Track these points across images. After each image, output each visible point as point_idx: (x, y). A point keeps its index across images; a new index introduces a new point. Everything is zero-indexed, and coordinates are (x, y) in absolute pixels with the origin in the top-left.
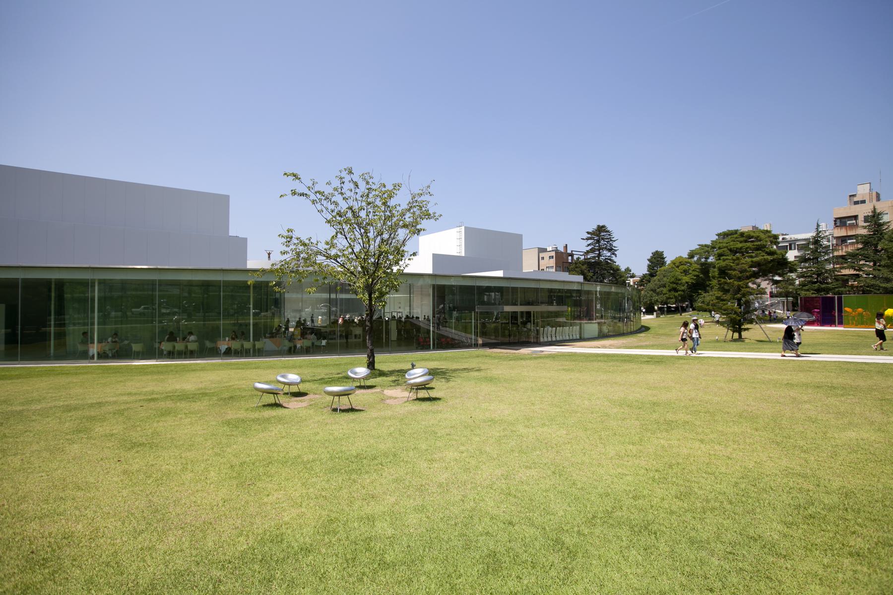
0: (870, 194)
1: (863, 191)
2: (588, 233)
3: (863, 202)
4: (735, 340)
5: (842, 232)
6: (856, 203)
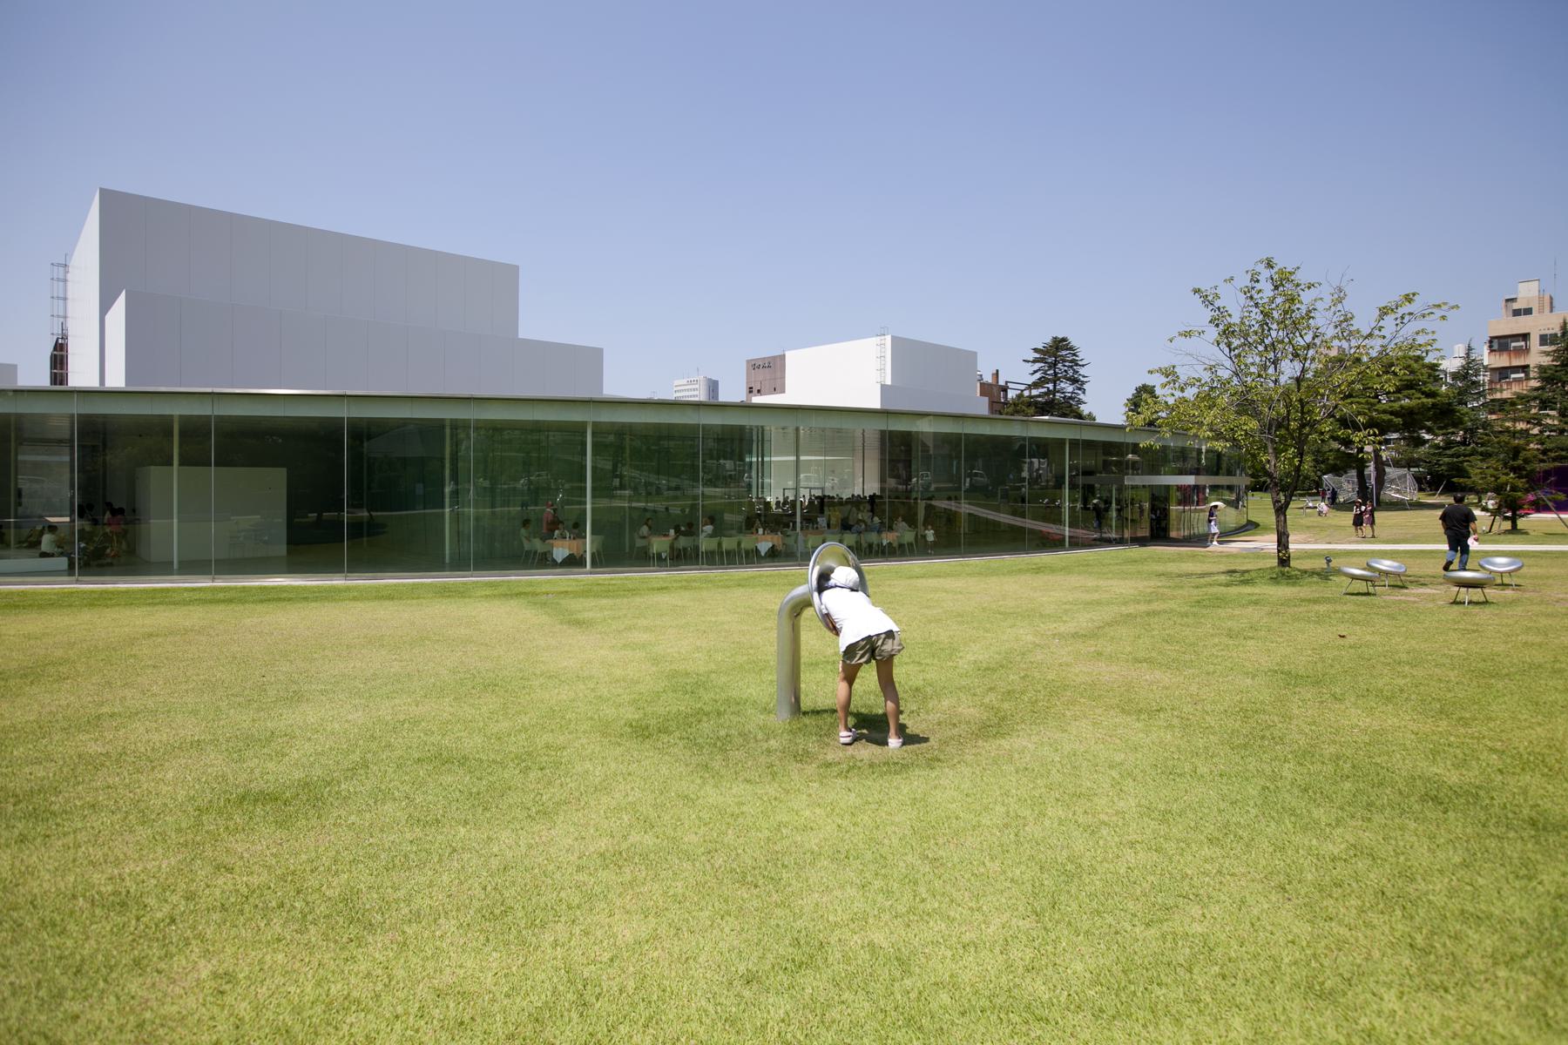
0: (1541, 299)
1: (1527, 293)
2: (1036, 350)
3: (1528, 311)
4: (1507, 532)
5: (1502, 361)
6: (1517, 313)
